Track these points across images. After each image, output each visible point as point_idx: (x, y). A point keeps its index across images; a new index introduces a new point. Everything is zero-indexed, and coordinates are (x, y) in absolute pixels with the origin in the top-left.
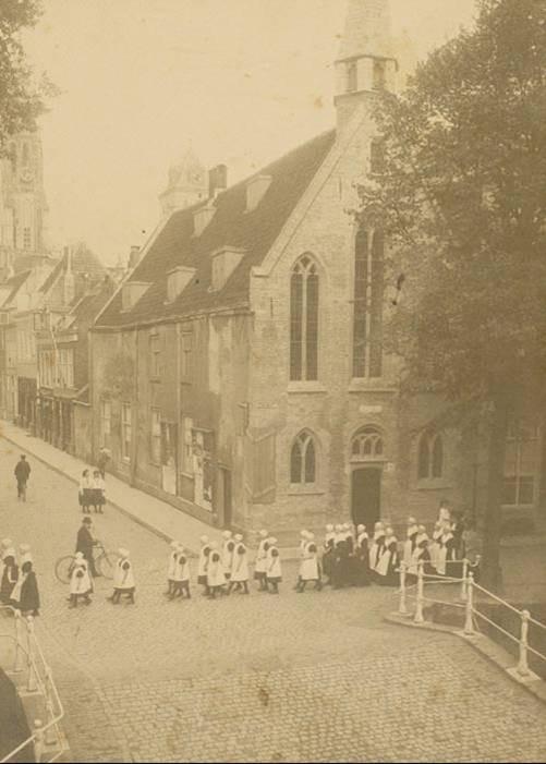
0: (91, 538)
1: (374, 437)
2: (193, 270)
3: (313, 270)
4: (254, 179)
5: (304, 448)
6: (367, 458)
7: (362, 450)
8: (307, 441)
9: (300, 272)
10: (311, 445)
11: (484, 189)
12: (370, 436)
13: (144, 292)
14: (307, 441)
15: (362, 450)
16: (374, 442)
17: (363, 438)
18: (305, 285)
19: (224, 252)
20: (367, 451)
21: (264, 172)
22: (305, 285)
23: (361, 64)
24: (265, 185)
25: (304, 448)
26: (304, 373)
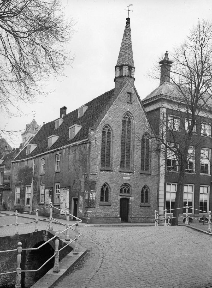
0: (200, 161)
1: (127, 188)
2: (58, 137)
3: (109, 130)
4: (82, 108)
5: (105, 190)
6: (125, 194)
7: (123, 192)
8: (106, 187)
9: (105, 131)
10: (107, 189)
11: (90, 129)
12: (126, 187)
13: (57, 139)
14: (106, 187)
15: (123, 192)
16: (127, 190)
17: (127, 188)
18: (107, 134)
19: (52, 137)
20: (125, 192)
21: (86, 105)
22: (107, 134)
23: (124, 68)
24: (85, 109)
25: (105, 190)
26: (106, 165)
